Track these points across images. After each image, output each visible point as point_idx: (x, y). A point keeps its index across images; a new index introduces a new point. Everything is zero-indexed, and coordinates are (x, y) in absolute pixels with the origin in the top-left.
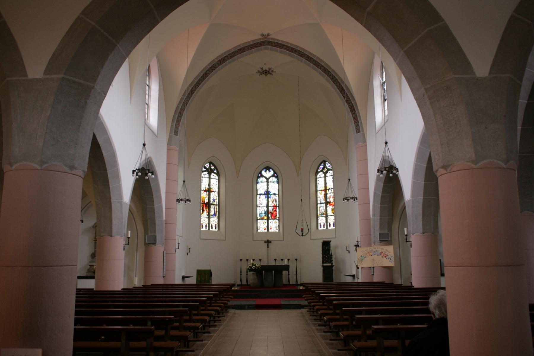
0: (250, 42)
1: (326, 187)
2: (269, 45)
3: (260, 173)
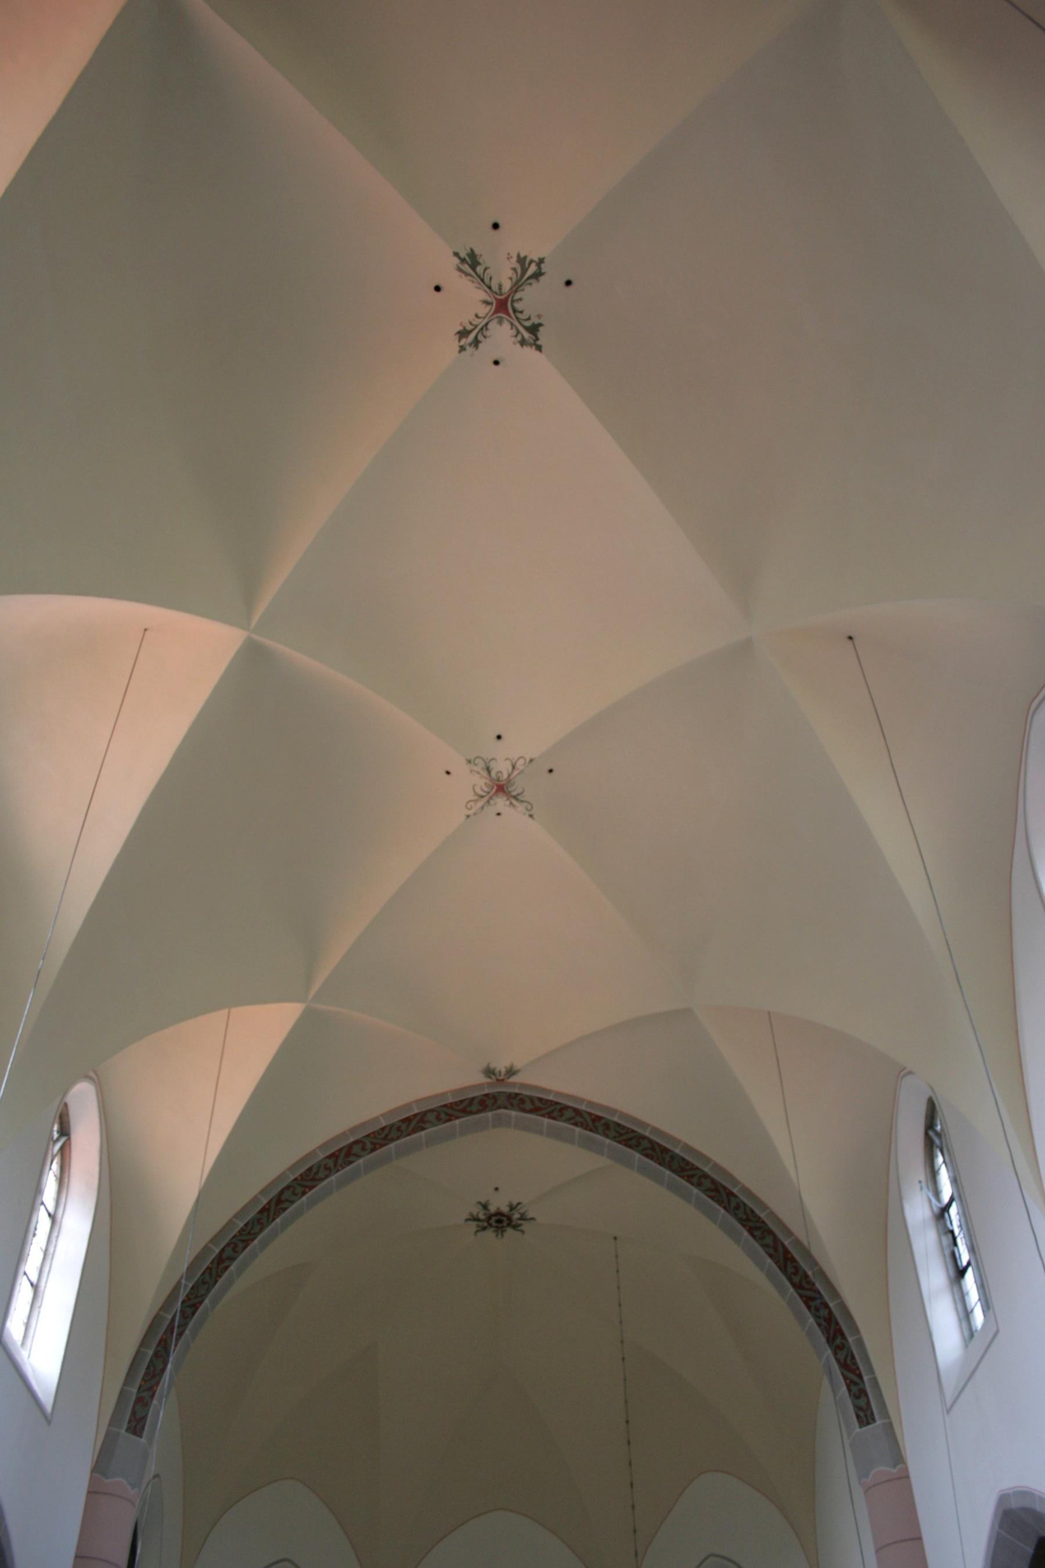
0: (443, 1095)
2: (512, 1107)
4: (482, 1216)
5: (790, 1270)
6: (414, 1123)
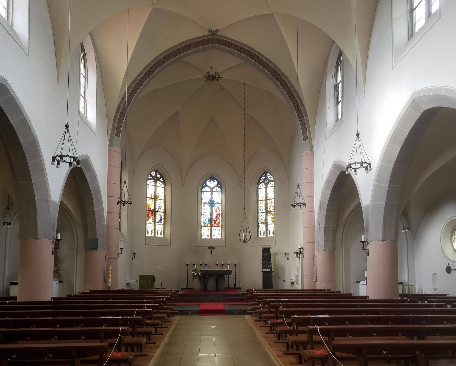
3: (205, 183)
4: (207, 76)
6: (187, 47)
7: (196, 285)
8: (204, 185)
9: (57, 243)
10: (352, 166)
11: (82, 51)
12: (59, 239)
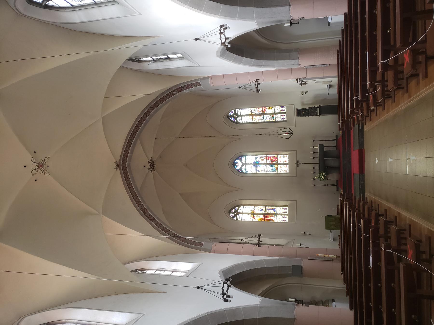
1: (249, 115)
3: (238, 170)
5: (166, 98)
7: (333, 177)
8: (240, 171)
9: (297, 302)
10: (223, 42)
11: (137, 271)
12: (294, 300)
